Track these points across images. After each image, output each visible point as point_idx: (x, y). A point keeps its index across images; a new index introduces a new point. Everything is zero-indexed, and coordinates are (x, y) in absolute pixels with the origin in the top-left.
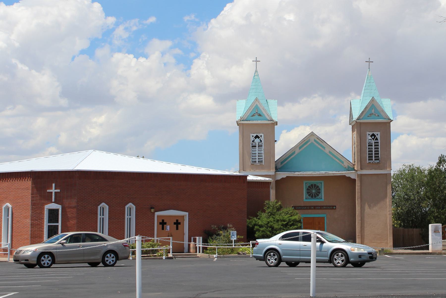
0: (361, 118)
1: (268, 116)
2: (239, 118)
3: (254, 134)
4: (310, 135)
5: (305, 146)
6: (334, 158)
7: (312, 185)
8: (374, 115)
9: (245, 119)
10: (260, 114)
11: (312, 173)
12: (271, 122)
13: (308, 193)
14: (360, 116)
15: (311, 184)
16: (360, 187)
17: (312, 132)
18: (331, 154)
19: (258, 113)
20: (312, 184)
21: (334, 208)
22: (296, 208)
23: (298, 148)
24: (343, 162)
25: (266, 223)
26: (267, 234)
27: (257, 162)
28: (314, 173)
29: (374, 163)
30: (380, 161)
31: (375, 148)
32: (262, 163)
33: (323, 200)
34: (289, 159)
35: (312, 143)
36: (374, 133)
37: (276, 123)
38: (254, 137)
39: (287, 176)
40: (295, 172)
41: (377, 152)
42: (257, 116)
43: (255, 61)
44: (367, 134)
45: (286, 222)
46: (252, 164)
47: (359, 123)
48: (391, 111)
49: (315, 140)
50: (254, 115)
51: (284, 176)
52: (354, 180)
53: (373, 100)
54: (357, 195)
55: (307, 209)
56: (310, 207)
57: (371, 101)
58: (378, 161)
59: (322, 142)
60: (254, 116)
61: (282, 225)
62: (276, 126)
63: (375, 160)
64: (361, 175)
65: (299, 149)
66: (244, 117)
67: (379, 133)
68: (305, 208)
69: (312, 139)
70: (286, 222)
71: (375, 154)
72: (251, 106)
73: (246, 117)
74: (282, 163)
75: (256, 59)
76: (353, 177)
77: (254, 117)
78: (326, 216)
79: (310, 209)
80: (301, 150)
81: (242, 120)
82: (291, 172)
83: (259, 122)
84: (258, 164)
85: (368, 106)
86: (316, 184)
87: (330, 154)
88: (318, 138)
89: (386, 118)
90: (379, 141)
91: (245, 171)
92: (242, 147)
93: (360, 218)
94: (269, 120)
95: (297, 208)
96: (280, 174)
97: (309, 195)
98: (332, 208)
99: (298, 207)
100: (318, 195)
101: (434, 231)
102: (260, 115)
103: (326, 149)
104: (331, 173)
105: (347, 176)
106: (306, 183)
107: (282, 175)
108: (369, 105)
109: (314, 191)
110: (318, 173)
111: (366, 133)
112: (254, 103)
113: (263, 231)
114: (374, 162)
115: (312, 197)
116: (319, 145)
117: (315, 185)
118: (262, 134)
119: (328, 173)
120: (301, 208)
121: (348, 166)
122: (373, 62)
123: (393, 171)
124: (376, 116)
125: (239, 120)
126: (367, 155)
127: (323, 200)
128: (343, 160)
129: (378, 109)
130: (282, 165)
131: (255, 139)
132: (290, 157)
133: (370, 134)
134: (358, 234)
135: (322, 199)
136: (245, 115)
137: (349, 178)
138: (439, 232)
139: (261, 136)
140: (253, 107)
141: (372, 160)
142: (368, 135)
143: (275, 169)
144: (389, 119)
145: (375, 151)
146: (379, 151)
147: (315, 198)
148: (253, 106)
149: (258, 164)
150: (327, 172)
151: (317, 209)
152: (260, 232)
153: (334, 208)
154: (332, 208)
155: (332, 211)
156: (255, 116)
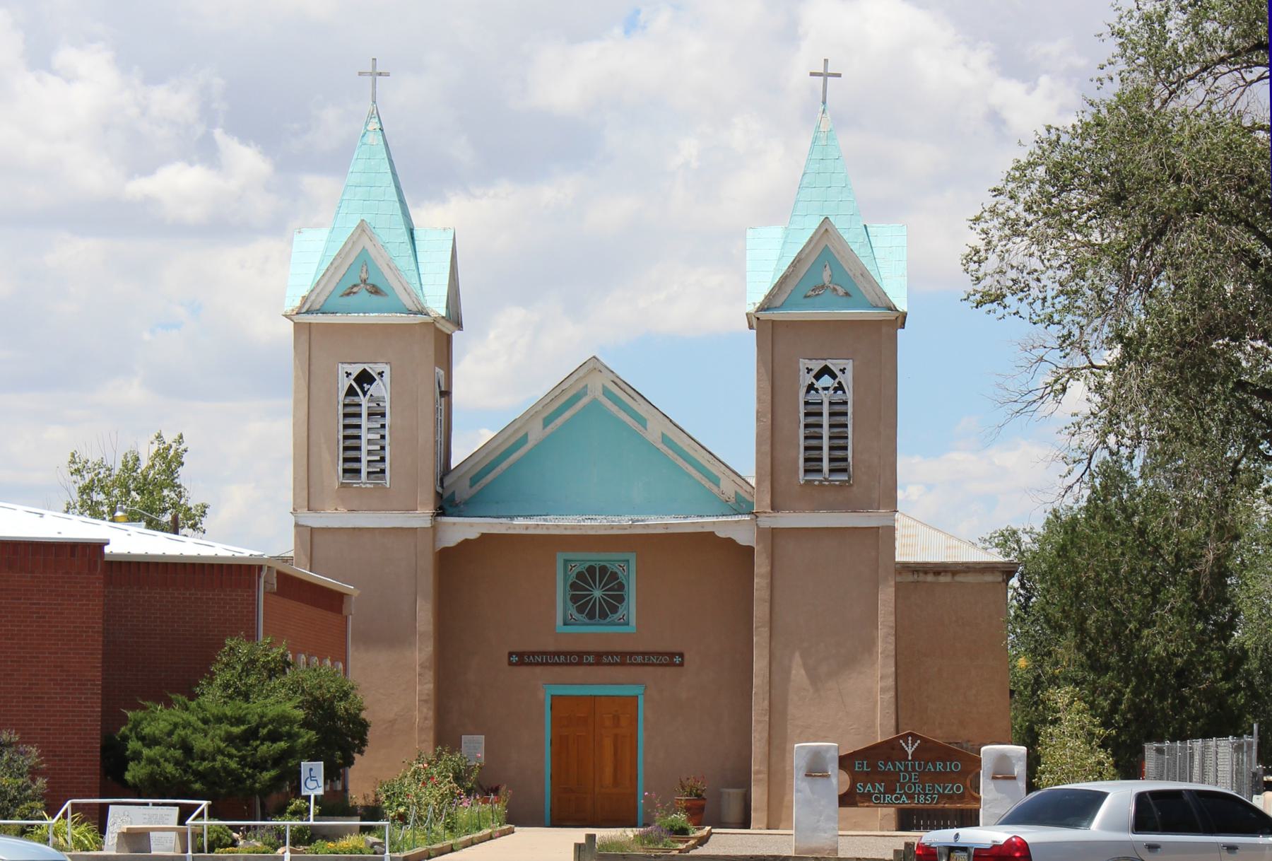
0: (778, 303)
1: (409, 294)
2: (298, 303)
3: (353, 365)
4: (585, 370)
5: (567, 415)
6: (680, 462)
7: (591, 570)
8: (828, 291)
9: (318, 307)
10: (380, 285)
11: (579, 521)
12: (420, 319)
13: (575, 599)
14: (771, 297)
15: (587, 565)
16: (769, 581)
17: (594, 357)
18: (670, 448)
19: (368, 282)
20: (593, 564)
21: (677, 660)
22: (526, 657)
23: (538, 423)
24: (716, 481)
25: (166, 730)
26: (164, 769)
27: (364, 474)
28: (588, 523)
29: (826, 483)
30: (849, 478)
31: (831, 426)
32: (384, 478)
33: (632, 628)
34: (504, 465)
35: (595, 401)
36: (829, 363)
37: (901, 320)
38: (353, 377)
39: (483, 534)
40: (512, 518)
41: (841, 442)
42: (363, 296)
43: (371, 74)
44: (801, 368)
45: (242, 727)
46: (342, 483)
47: (770, 325)
48: (906, 274)
49: (606, 392)
50: (355, 290)
51: (473, 534)
52: (749, 551)
53: (825, 229)
54: (760, 611)
55: (571, 664)
56: (580, 654)
57: (818, 237)
58: (844, 477)
59: (633, 398)
60: (354, 293)
61: (230, 739)
62: (900, 331)
63: (832, 471)
64: (774, 531)
65: (541, 426)
66: (313, 298)
67: (849, 365)
68: (562, 658)
69: (596, 385)
70: (242, 727)
71: (831, 448)
72: (343, 255)
73: (322, 299)
74: (474, 480)
75: (374, 67)
76: (745, 537)
77: (352, 298)
78: (642, 692)
79: (580, 664)
80: (552, 427)
81: (304, 310)
82: (498, 517)
83: (373, 318)
84: (368, 486)
85: (803, 256)
86: (608, 565)
87: (667, 449)
88: (618, 382)
89: (880, 305)
90: (849, 396)
91: (315, 511)
92: (306, 418)
93: (766, 703)
94: (410, 312)
95: (529, 658)
96: (454, 524)
97: (580, 610)
98: (672, 659)
99: (533, 654)
100: (614, 610)
101: (994, 774)
102: (376, 291)
103: (649, 425)
104: (657, 522)
105: (721, 534)
106: (566, 561)
107: (461, 529)
108: (810, 252)
109: (598, 594)
110: (605, 522)
111: (798, 362)
112: (352, 241)
113: (151, 761)
114: (826, 480)
115: (591, 616)
116: (620, 408)
117: (603, 570)
118: (384, 365)
119: (642, 521)
120: (542, 660)
121: (736, 492)
122: (839, 75)
123: (1045, 512)
124: (837, 294)
125: (293, 310)
126: (798, 453)
127: (632, 628)
128: (715, 473)
129: (846, 269)
130: (477, 487)
131: (817, 380)
132: (508, 456)
133: (811, 370)
134: (757, 768)
135: (628, 624)
136: (318, 290)
137: (730, 542)
138: (1014, 778)
139: (379, 374)
140: (351, 259)
141: (820, 471)
142: (803, 371)
143: (432, 506)
144: (890, 309)
145: (831, 438)
146: (846, 438)
147: (602, 621)
148: (348, 254)
149: (368, 486)
150: (638, 521)
151: (609, 664)
152: (143, 763)
153: (677, 660)
154: (672, 659)
155: (669, 671)
156: (355, 296)
